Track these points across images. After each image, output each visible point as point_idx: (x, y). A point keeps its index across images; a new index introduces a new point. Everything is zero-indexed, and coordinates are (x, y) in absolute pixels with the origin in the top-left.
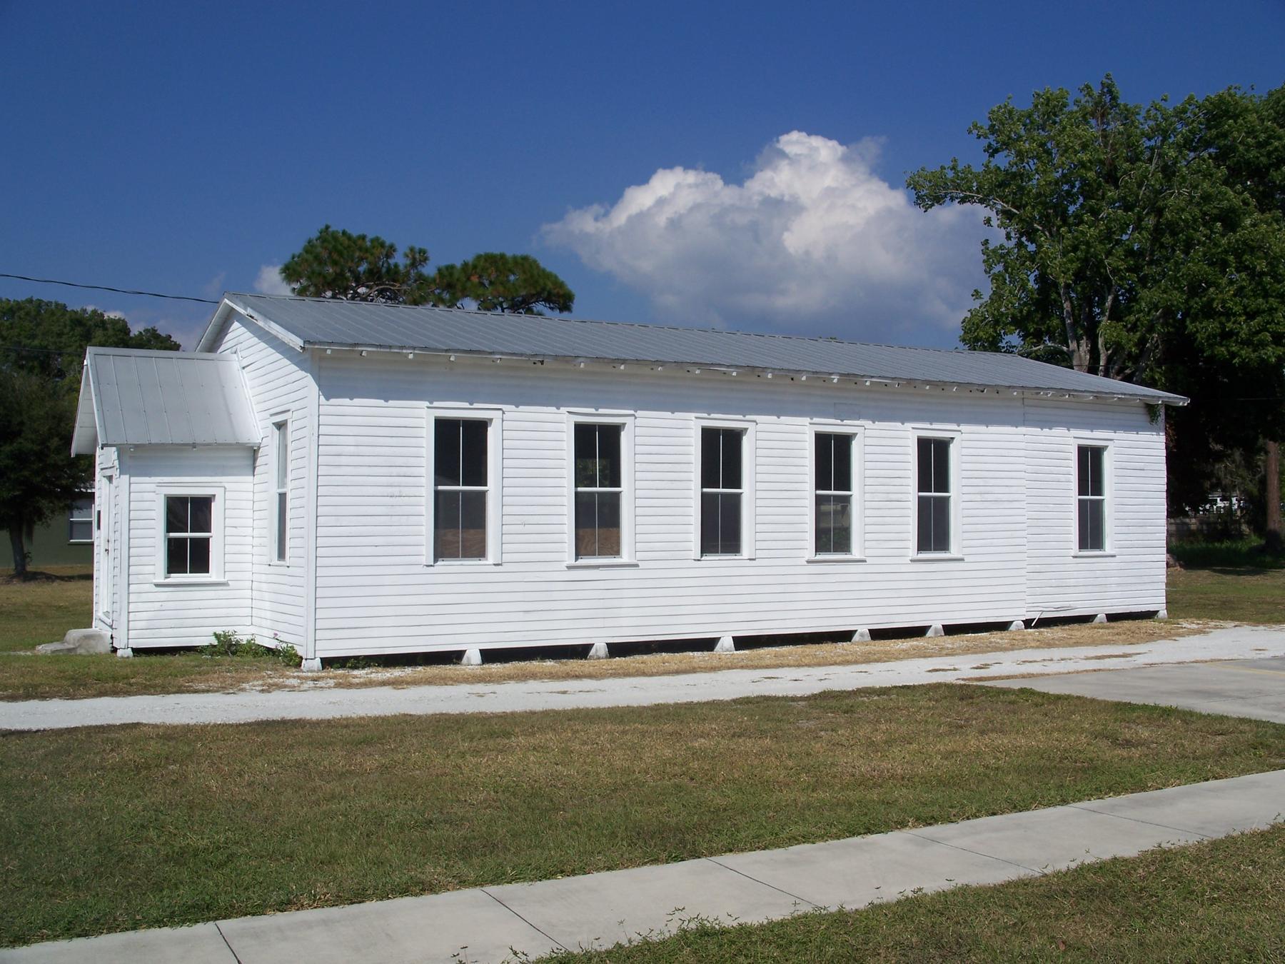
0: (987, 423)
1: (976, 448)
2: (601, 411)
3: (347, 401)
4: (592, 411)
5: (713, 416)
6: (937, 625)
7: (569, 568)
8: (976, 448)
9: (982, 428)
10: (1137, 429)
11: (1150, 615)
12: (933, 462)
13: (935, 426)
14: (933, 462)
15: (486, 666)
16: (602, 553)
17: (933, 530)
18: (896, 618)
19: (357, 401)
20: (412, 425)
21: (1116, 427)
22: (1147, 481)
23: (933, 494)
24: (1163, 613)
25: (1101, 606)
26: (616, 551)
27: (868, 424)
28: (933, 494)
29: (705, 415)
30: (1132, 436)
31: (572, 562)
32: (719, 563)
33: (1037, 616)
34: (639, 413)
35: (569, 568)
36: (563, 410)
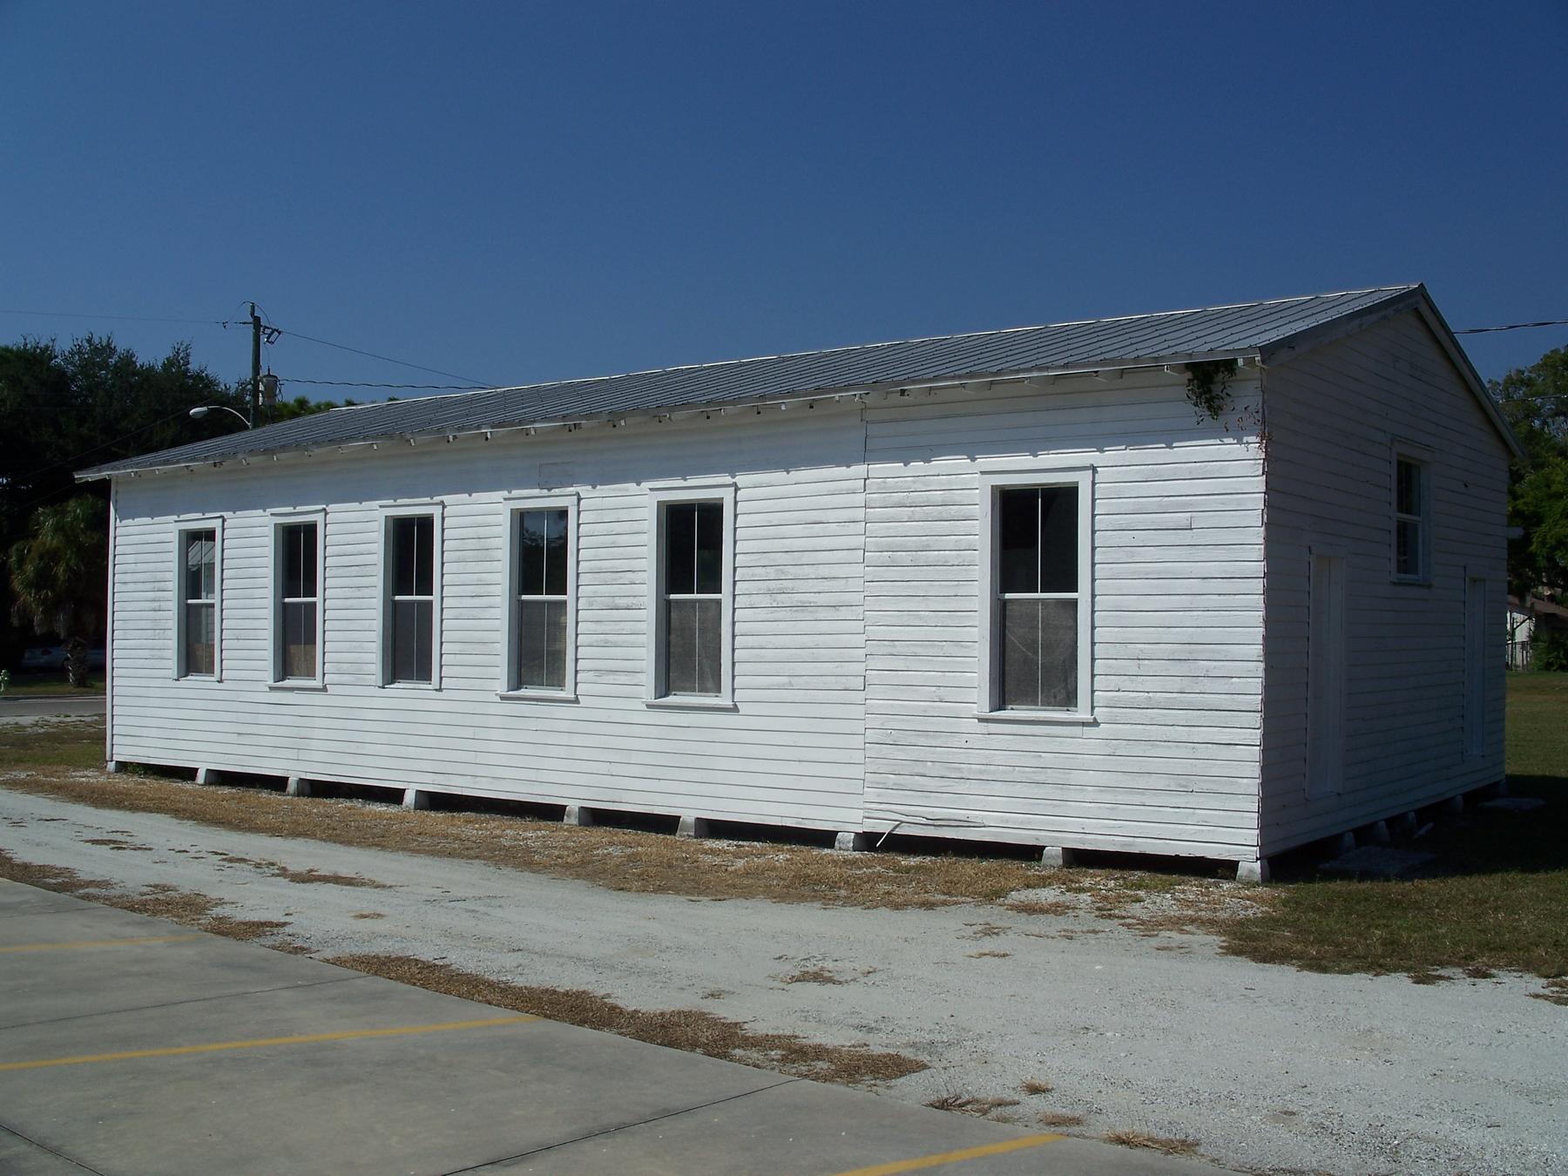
0: (787, 467)
1: (777, 513)
2: (299, 509)
3: (355, 505)
4: (290, 509)
5: (400, 501)
6: (573, 806)
7: (272, 689)
8: (777, 513)
9: (779, 476)
10: (1169, 436)
11: (1225, 869)
12: (691, 546)
13: (692, 482)
14: (691, 546)
15: (212, 788)
16: (1050, 702)
17: (687, 657)
18: (626, 796)
19: (796, 475)
20: (959, 492)
21: (1099, 442)
22: (1201, 554)
23: (414, 598)
24: (1251, 866)
25: (1060, 829)
26: (1070, 700)
27: (584, 490)
28: (414, 598)
29: (391, 502)
30: (1155, 454)
31: (271, 682)
32: (404, 691)
33: (885, 828)
34: (741, 479)
35: (272, 689)
36: (646, 485)
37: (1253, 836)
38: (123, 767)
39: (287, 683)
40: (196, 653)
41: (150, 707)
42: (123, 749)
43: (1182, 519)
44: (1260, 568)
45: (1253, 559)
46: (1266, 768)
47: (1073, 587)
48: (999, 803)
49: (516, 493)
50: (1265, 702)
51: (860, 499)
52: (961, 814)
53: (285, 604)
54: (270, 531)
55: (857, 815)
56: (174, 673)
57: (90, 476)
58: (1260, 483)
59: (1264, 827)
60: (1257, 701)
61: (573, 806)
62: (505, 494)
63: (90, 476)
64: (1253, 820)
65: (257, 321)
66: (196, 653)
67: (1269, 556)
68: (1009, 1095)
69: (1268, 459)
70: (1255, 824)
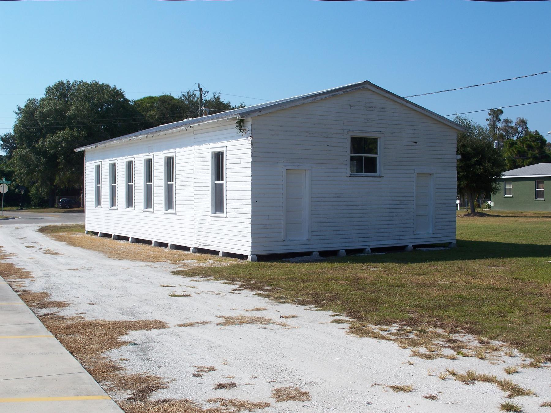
18: (161, 238)
24: (250, 257)
27: (154, 153)
37: (249, 248)
38: (88, 232)
39: (148, 210)
40: (98, 202)
41: (97, 216)
42: (89, 228)
43: (238, 161)
44: (250, 174)
45: (248, 172)
46: (252, 229)
47: (222, 180)
48: (213, 239)
49: (145, 154)
50: (252, 211)
51: (192, 156)
52: (207, 242)
53: (216, 184)
54: (94, 167)
55: (193, 243)
56: (94, 205)
57: (78, 150)
58: (250, 151)
59: (252, 246)
60: (250, 211)
61: (154, 241)
62: (143, 155)
63: (78, 150)
64: (249, 244)
65: (201, 89)
66: (98, 202)
67: (253, 171)
68: (524, 370)
69: (252, 143)
70: (250, 245)
